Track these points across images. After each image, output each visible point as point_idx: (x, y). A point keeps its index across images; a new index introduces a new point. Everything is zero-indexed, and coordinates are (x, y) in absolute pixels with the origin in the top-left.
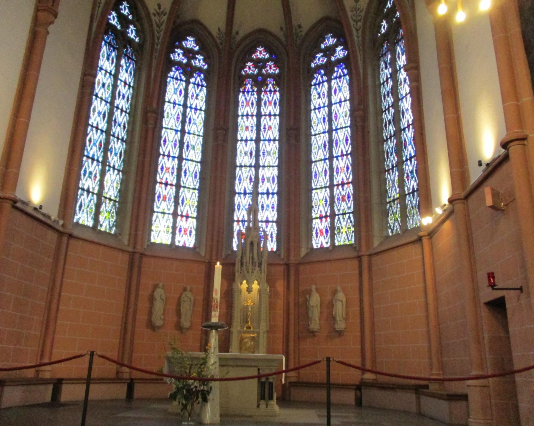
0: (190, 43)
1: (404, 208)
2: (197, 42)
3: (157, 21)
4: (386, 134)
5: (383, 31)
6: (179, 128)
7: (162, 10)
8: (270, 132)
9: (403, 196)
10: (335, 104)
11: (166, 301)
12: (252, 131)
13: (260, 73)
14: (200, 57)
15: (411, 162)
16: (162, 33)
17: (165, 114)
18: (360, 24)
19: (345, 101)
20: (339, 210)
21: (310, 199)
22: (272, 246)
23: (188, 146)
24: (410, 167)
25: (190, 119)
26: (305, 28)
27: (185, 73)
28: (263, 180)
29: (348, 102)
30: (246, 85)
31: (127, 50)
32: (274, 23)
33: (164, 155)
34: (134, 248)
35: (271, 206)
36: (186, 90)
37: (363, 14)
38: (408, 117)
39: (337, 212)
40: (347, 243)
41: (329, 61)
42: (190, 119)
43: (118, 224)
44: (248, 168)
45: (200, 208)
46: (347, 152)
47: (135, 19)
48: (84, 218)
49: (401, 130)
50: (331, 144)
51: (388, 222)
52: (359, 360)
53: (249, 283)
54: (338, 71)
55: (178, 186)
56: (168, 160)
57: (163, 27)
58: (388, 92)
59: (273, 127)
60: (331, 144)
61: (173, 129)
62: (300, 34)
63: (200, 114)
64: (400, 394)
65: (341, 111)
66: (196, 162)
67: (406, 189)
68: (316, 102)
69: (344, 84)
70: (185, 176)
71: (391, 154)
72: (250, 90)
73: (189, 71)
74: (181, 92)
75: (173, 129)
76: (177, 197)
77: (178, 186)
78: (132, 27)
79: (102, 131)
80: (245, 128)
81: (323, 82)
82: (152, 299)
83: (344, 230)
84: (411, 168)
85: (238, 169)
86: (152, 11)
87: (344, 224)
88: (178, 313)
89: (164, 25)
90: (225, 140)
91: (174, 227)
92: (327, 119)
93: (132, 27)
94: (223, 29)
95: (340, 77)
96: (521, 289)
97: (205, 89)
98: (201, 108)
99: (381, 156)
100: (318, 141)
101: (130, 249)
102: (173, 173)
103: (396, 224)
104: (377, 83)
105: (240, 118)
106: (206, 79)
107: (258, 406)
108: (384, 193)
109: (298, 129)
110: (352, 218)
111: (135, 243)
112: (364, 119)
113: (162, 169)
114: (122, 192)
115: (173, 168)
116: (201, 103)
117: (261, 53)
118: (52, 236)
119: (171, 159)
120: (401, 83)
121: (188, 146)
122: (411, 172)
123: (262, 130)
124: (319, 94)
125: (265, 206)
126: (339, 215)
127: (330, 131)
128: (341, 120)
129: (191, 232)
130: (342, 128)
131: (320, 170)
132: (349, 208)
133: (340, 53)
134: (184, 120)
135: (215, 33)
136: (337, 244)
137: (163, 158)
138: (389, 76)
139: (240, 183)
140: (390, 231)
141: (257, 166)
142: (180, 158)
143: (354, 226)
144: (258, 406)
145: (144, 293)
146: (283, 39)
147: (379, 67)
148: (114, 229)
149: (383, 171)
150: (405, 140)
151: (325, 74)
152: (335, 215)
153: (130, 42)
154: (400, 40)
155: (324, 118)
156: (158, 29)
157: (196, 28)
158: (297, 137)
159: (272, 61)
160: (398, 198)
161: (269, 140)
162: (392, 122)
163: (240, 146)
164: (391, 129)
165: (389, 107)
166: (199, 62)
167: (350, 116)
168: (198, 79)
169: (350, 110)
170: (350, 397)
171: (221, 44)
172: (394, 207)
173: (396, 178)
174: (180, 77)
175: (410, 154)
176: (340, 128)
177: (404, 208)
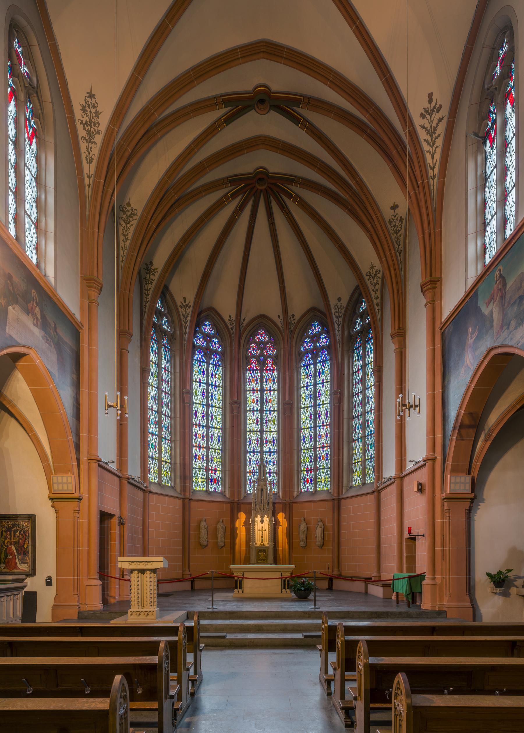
0: (207, 328)
1: (364, 469)
3: (184, 313)
4: (355, 413)
5: (358, 328)
6: (205, 403)
7: (187, 303)
8: (270, 404)
9: (364, 461)
10: (319, 384)
11: (207, 529)
12: (257, 403)
13: (261, 354)
14: (215, 340)
15: (371, 437)
16: (188, 324)
17: (194, 392)
18: (341, 320)
19: (327, 382)
20: (320, 466)
21: (299, 457)
22: (275, 490)
23: (212, 417)
24: (370, 440)
25: (212, 395)
26: (297, 318)
27: (205, 355)
28: (266, 442)
29: (328, 384)
30: (251, 364)
31: (164, 340)
33: (196, 425)
34: (184, 495)
35: (272, 461)
36: (207, 369)
37: (343, 311)
38: (372, 404)
39: (318, 467)
40: (325, 489)
41: (315, 348)
42: (212, 395)
44: (256, 433)
45: (223, 464)
46: (327, 423)
47: (166, 311)
48: (152, 477)
49: (366, 413)
50: (315, 416)
51: (353, 477)
53: (262, 517)
54: (322, 356)
55: (208, 448)
56: (199, 428)
57: (189, 318)
58: (359, 380)
59: (272, 400)
60: (315, 416)
61: (200, 404)
62: (293, 322)
63: (219, 390)
64: (356, 583)
65: (323, 390)
66: (218, 429)
67: (366, 455)
68: (305, 381)
69: (327, 367)
70: (212, 440)
71: (358, 429)
72: (255, 369)
73: (208, 353)
74: (204, 372)
75: (200, 404)
76: (207, 456)
77: (208, 448)
78: (165, 319)
79: (155, 411)
80: (252, 399)
81: (310, 364)
82: (199, 528)
83: (323, 480)
84: (370, 442)
85: (248, 433)
86: (179, 304)
87: (323, 476)
88: (216, 537)
89: (189, 316)
90: (239, 411)
91: (207, 479)
92: (313, 395)
93: (165, 319)
94: (234, 317)
95: (323, 361)
96: (423, 535)
97: (221, 368)
98: (219, 384)
99: (351, 430)
100: (306, 413)
101: (182, 496)
102: (203, 438)
103: (359, 479)
104: (351, 372)
105: (248, 392)
106: (221, 359)
107: (282, 592)
108: (351, 457)
109: (292, 404)
110: (329, 472)
111: (185, 491)
112: (340, 400)
113: (196, 435)
114: (173, 456)
115: (203, 435)
116: (218, 381)
117: (262, 336)
118: (140, 493)
119: (201, 427)
120: (368, 375)
121: (212, 417)
122: (371, 444)
123: (265, 402)
124: (307, 374)
125: (268, 461)
126: (320, 469)
127: (315, 406)
128: (323, 397)
129: (218, 481)
130: (324, 404)
131: (307, 436)
132: (327, 465)
133: (324, 341)
134: (207, 395)
135: (226, 319)
136: (318, 489)
137: (196, 427)
138: (360, 368)
139: (250, 444)
140: (354, 482)
141: (262, 431)
142: (208, 427)
143: (330, 477)
144: (282, 592)
146: (280, 325)
147: (353, 359)
148: (170, 482)
149: (351, 441)
150: (368, 421)
151: (312, 358)
152: (318, 469)
153: (165, 332)
154: (370, 339)
155: (311, 395)
156: (184, 320)
158: (291, 410)
159: (271, 343)
160: (360, 461)
161: (270, 411)
162: (360, 405)
163: (249, 415)
164: (359, 410)
165: (358, 393)
166: (215, 345)
167: (330, 395)
168: (215, 359)
169: (330, 390)
170: (325, 584)
171: (232, 329)
172: (357, 466)
173: (361, 447)
174: (203, 359)
175: (371, 431)
176: (322, 404)
177: (364, 469)
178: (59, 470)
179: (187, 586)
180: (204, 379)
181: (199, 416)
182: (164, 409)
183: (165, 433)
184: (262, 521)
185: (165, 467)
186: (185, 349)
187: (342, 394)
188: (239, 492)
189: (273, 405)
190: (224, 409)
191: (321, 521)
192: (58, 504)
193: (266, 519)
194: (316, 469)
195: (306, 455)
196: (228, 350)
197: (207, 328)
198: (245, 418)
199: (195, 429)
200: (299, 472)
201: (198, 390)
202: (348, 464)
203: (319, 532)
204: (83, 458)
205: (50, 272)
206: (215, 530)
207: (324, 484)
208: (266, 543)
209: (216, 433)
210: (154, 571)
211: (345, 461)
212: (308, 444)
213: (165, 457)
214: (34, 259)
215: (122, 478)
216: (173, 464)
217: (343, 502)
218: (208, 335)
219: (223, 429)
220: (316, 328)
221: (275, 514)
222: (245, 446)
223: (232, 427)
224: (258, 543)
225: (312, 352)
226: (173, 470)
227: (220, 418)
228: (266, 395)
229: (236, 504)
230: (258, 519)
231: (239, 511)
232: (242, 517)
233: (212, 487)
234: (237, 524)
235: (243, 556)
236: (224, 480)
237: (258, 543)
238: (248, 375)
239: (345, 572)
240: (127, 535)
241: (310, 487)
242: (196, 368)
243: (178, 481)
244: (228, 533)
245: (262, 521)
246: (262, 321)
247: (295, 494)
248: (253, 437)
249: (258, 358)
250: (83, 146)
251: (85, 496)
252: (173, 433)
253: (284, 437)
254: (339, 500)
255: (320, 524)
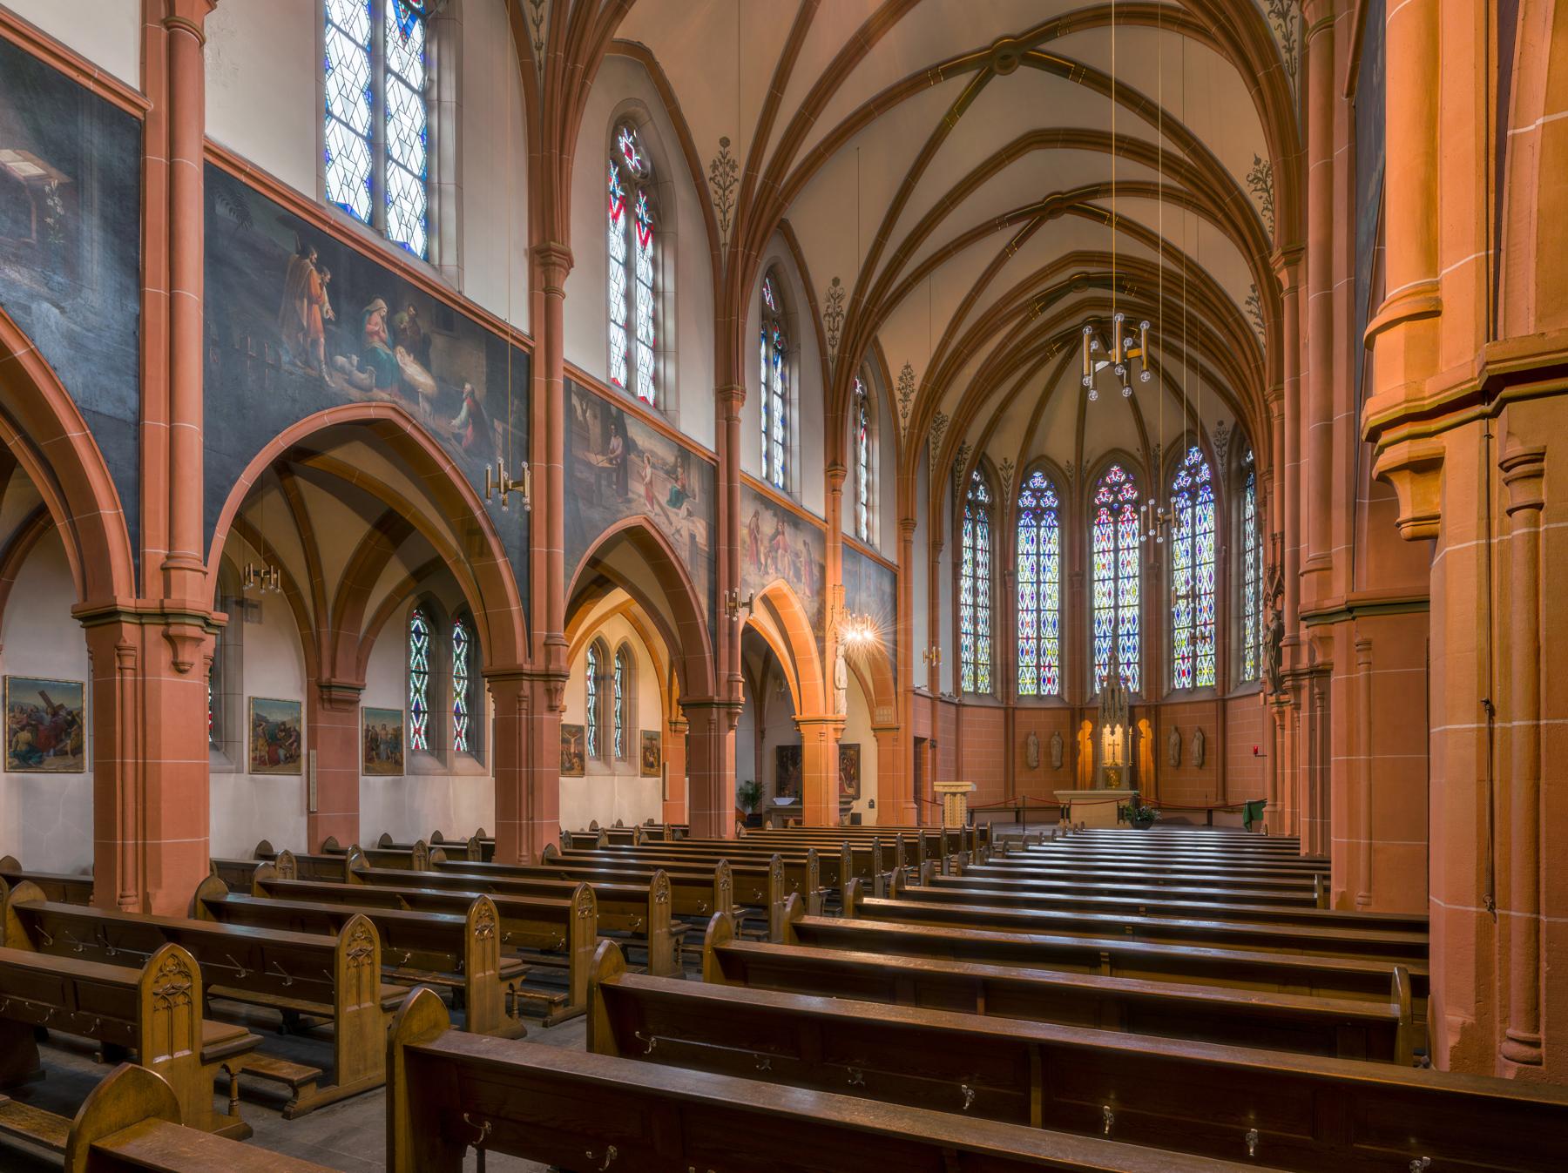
0: (1038, 480)
2: (1046, 476)
11: (1038, 745)
14: (1049, 493)
21: (1171, 640)
22: (1134, 687)
32: (1129, 439)
36: (1038, 536)
41: (1194, 484)
43: (993, 684)
45: (1061, 657)
48: (967, 686)
52: (487, 1159)
53: (1113, 728)
54: (1204, 495)
69: (1210, 511)
77: (1039, 639)
80: (1101, 566)
82: (1026, 744)
91: (1038, 679)
94: (1073, 463)
106: (1057, 518)
109: (1160, 568)
114: (992, 656)
116: (1053, 547)
117: (1116, 475)
127: (1194, 566)
128: (1205, 554)
134: (1038, 569)
135: (1063, 465)
145: (1019, 740)
157: (1045, 463)
158: (1158, 577)
163: (1098, 587)
166: (1050, 500)
168: (1050, 519)
170: (1203, 819)
178: (879, 703)
179: (1011, 816)
180: (1033, 549)
181: (1027, 598)
182: (981, 599)
183: (982, 629)
184: (1113, 733)
185: (982, 670)
186: (1006, 519)
187: (1228, 552)
188: (1083, 694)
189: (1134, 569)
190: (1061, 583)
191: (1200, 730)
192: (879, 734)
193: (1119, 729)
194: (1195, 656)
195: (1182, 636)
196: (1067, 504)
197: (1038, 480)
198: (1092, 591)
199: (1022, 616)
200: (1171, 661)
201: (1025, 565)
202: (1238, 650)
203: (1195, 747)
204: (901, 689)
205: (877, 541)
206: (1049, 746)
207: (1207, 677)
208: (1119, 761)
209: (1051, 617)
210: (964, 794)
211: (1234, 645)
212: (1184, 621)
213: (983, 658)
214: (418, 243)
215: (935, 700)
216: (993, 665)
217: (1231, 704)
218: (1039, 490)
219: (1061, 611)
220: (1195, 456)
221: (1132, 722)
222: (1092, 629)
223: (1072, 606)
224: (1108, 761)
225: (1188, 490)
226: (992, 674)
227: (1056, 596)
228: (1122, 556)
229: (1078, 708)
230: (1107, 730)
231: (1082, 719)
232: (1088, 727)
233: (1046, 689)
234: (1080, 738)
235: (1089, 779)
236: (1061, 678)
237: (1108, 761)
238: (1096, 531)
239: (1231, 801)
240: (939, 757)
241: (1186, 682)
242: (1022, 537)
243: (999, 686)
244: (1067, 749)
245: (1113, 733)
246: (1115, 455)
247: (1165, 691)
248: (1103, 615)
249: (1109, 506)
250: (900, 406)
251: (902, 725)
252: (992, 627)
253: (1148, 614)
254: (1224, 701)
255: (1198, 734)
